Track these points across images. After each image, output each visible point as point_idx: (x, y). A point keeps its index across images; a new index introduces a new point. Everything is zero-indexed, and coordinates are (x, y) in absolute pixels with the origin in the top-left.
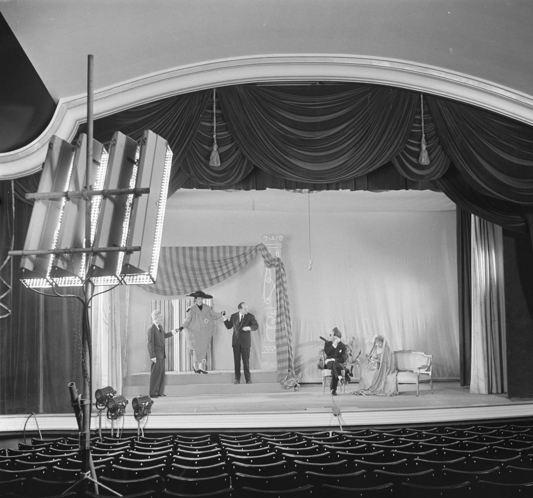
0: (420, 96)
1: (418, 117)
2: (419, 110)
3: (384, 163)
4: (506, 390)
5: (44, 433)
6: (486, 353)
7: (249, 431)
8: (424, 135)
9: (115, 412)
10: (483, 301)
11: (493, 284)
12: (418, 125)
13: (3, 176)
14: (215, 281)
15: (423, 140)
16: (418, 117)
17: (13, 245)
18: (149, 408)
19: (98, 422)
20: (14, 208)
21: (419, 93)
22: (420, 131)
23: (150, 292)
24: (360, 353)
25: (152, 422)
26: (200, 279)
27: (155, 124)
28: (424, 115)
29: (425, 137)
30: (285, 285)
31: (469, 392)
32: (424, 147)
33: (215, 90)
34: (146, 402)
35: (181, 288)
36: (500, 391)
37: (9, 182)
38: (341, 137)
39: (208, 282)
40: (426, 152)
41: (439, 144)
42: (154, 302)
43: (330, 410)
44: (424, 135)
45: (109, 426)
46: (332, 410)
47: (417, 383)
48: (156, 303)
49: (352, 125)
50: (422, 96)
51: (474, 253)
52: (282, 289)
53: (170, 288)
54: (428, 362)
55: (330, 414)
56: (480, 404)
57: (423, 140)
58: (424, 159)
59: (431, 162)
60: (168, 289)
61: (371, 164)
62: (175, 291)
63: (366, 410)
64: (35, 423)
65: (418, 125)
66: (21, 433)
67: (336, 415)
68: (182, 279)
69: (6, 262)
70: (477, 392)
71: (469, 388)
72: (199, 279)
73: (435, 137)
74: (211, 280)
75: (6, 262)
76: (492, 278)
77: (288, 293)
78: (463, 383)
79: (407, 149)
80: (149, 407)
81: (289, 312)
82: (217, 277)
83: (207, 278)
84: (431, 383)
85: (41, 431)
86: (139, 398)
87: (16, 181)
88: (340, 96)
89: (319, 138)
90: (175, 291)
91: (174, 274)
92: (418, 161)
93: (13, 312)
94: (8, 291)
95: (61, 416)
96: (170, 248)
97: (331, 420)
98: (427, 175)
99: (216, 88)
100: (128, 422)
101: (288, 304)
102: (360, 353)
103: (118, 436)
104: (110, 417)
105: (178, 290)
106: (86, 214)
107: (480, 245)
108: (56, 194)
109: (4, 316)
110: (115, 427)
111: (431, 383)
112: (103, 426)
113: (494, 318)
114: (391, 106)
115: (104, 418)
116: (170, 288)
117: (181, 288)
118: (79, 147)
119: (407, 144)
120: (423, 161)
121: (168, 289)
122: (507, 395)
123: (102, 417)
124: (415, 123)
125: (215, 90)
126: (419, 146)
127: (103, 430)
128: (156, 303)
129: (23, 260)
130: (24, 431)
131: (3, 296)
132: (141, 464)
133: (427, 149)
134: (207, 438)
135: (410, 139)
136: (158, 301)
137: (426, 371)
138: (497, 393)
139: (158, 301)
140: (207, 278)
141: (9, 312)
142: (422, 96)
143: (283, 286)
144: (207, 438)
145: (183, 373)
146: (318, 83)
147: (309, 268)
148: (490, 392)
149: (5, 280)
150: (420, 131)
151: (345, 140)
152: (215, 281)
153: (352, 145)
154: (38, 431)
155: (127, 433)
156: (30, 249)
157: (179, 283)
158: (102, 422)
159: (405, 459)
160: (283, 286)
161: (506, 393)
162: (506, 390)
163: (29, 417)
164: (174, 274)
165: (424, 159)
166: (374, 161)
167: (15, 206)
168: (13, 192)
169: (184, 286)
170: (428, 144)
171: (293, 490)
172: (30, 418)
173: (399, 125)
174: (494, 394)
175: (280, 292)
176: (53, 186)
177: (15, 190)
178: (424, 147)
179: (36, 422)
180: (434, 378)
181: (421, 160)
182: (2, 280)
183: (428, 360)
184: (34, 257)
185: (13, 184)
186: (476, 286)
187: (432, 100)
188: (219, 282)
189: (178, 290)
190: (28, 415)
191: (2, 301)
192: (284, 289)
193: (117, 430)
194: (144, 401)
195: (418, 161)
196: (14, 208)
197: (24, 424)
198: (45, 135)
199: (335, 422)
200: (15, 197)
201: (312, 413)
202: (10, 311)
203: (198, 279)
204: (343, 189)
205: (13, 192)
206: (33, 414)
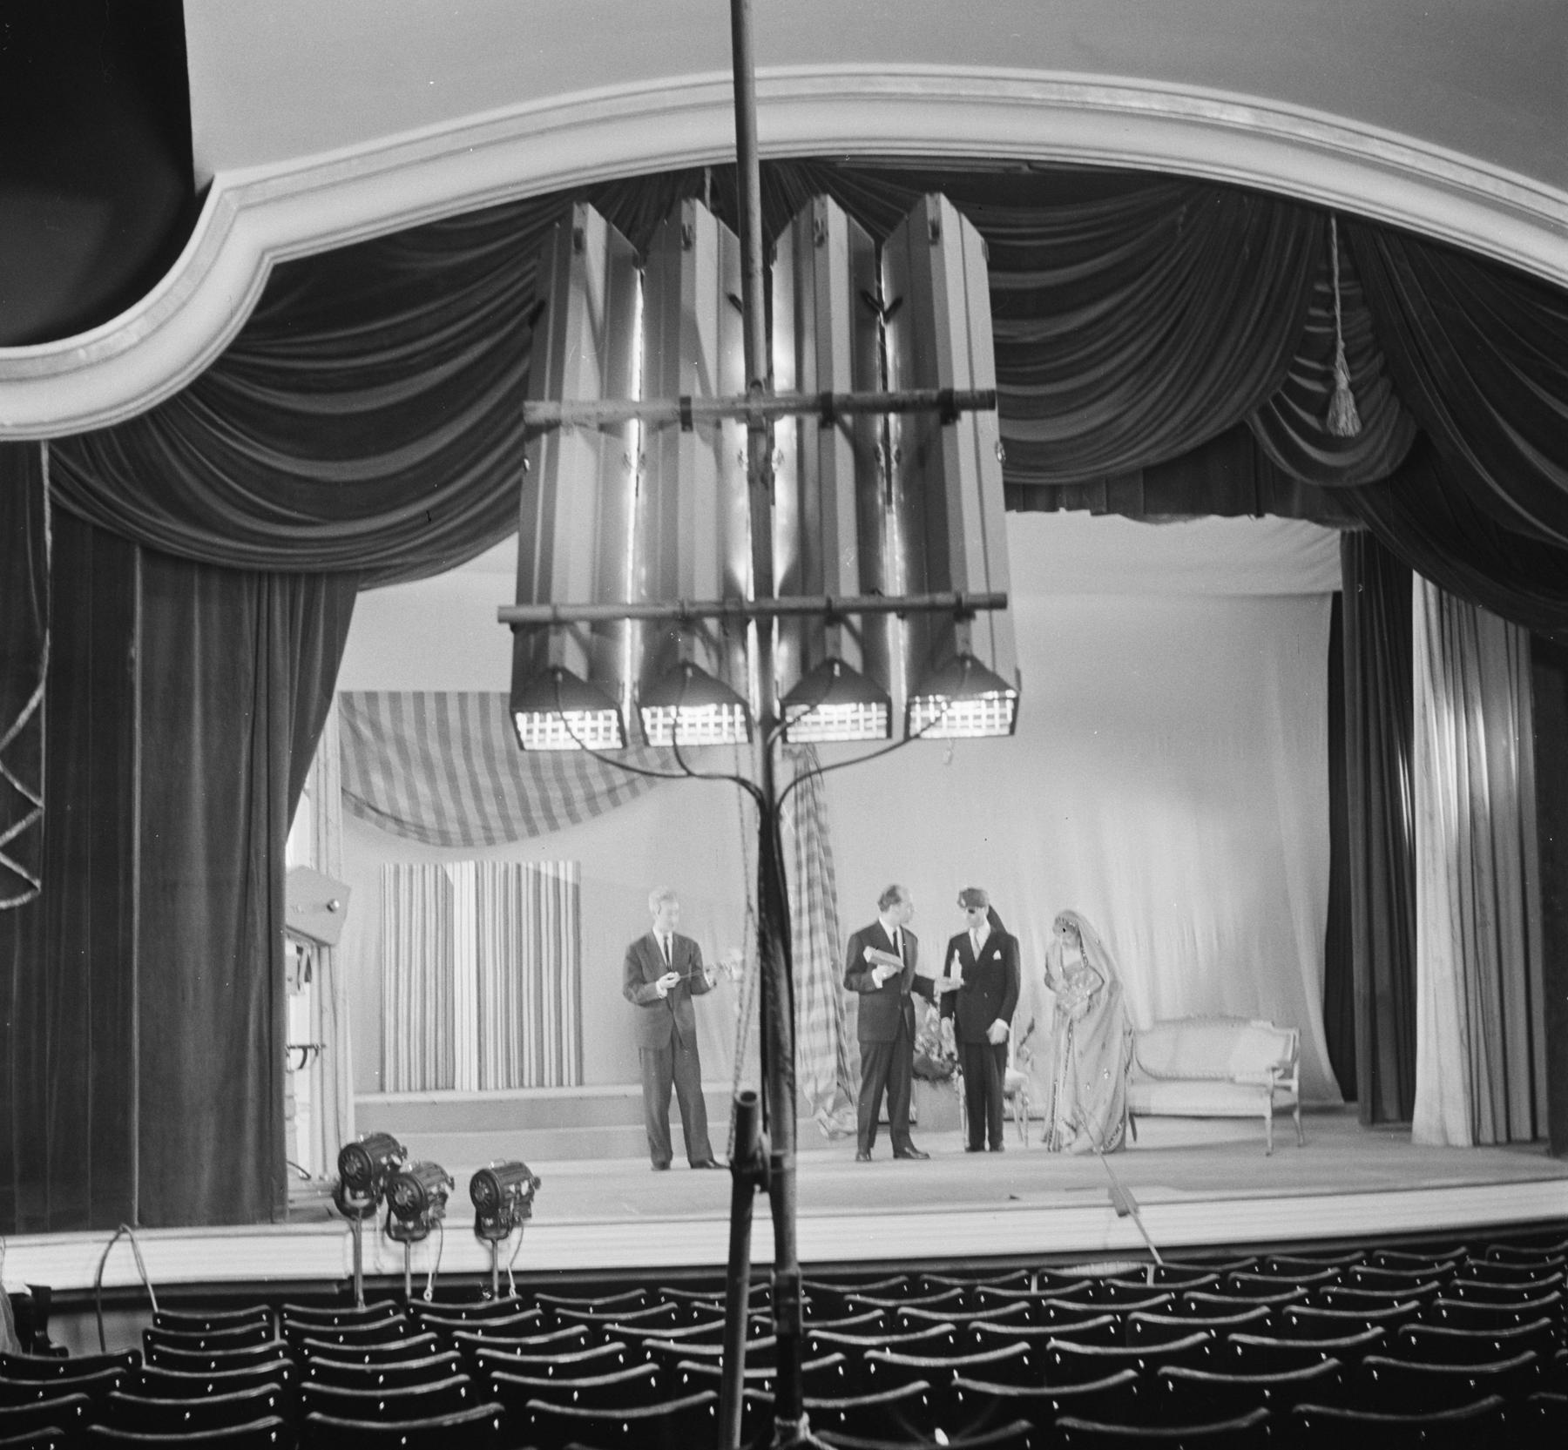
0: (1328, 222)
1: (1321, 287)
2: (1323, 267)
3: (1227, 426)
4: (1543, 1130)
5: (164, 1293)
6: (1463, 1023)
7: (896, 1269)
8: (1341, 344)
9: (414, 1218)
10: (1454, 867)
11: (1479, 813)
12: (1320, 313)
13: (16, 426)
14: (603, 802)
15: (1340, 358)
16: (1321, 287)
17: (46, 662)
18: (528, 1204)
19: (350, 1251)
20: (48, 536)
21: (1323, 212)
22: (1327, 330)
23: (400, 834)
24: (1031, 1029)
25: (538, 1247)
26: (559, 794)
27: (517, 275)
28: (1340, 281)
29: (1345, 351)
30: (822, 817)
31: (1408, 1141)
32: (1343, 380)
33: (708, 174)
34: (518, 1184)
35: (496, 824)
36: (1502, 1138)
37: (33, 447)
38: (1097, 340)
39: (580, 806)
40: (1351, 395)
41: (1384, 371)
42: (390, 868)
43: (1102, 1196)
44: (1341, 344)
45: (390, 1266)
46: (1111, 1196)
47: (1268, 1114)
48: (397, 873)
49: (1133, 303)
50: (1334, 223)
51: (1425, 717)
52: (814, 827)
53: (463, 822)
54: (1285, 1051)
55: (1103, 1210)
56: (1440, 1180)
57: (1340, 358)
58: (1346, 419)
59: (1364, 424)
60: (453, 828)
61: (1188, 427)
62: (477, 833)
63: (1212, 1195)
64: (133, 1261)
65: (1320, 313)
66: (134, 1294)
67: (1122, 1214)
68: (499, 793)
69: (24, 717)
70: (1436, 1140)
71: (1410, 1130)
72: (555, 794)
73: (1370, 352)
74: (591, 798)
75: (24, 717)
76: (1477, 793)
77: (832, 841)
78: (1369, 1116)
79: (1291, 387)
80: (525, 1202)
81: (834, 900)
82: (611, 791)
83: (578, 793)
84: (1296, 1115)
85: (156, 1287)
86: (496, 1170)
87: (56, 443)
88: (1094, 210)
89: (1031, 339)
90: (477, 833)
91: (473, 776)
92: (1323, 424)
93: (43, 886)
94: (32, 817)
95: (223, 1236)
96: (462, 696)
97: (1108, 1230)
98: (1352, 467)
99: (714, 168)
100: (453, 1248)
101: (831, 875)
102: (1031, 1029)
103: (428, 1295)
104: (418, 1234)
105: (487, 828)
106: (751, 481)
107: (1442, 694)
108: (608, 409)
109: (17, 902)
110: (503, 1263)
111: (1296, 1115)
112: (368, 1267)
113: (1484, 915)
114: (1247, 250)
115: (371, 1232)
116: (463, 822)
117: (496, 824)
118: (689, 244)
119: (1293, 371)
120: (1342, 424)
121: (453, 828)
122: (1548, 1146)
123: (364, 1235)
124: (1314, 305)
125: (708, 174)
126: (1328, 378)
127: (367, 1278)
128: (397, 873)
129: (553, 640)
130: (98, 1288)
131: (11, 834)
132: (210, 1388)
133: (1351, 385)
134: (256, 1317)
135: (1299, 355)
136: (404, 868)
137: (1282, 1077)
138: (1496, 1144)
139: (404, 868)
140: (578, 793)
141: (32, 887)
142: (1334, 223)
143: (817, 820)
144: (256, 1317)
145: (484, 1096)
146: (1026, 168)
147: (946, 759)
148: (1477, 1142)
149: (21, 780)
150: (1327, 330)
151: (1111, 349)
152: (603, 802)
153: (1131, 366)
154: (144, 1287)
155: (459, 1290)
156: (570, 601)
157: (491, 808)
158: (364, 1250)
159: (1531, 1354)
160: (817, 820)
161: (1544, 1141)
162: (1543, 1130)
163: (111, 1243)
164: (473, 776)
165: (1346, 419)
166: (1199, 418)
167: (52, 529)
168: (46, 482)
169: (505, 818)
170: (1352, 372)
171: (138, 1436)
172: (116, 1245)
173: (1134, 331)
174: (1488, 1145)
175: (809, 837)
176: (602, 381)
177: (51, 478)
178: (1343, 380)
179: (137, 1256)
180: (1305, 1102)
181: (1336, 421)
182: (10, 778)
183: (1287, 1044)
184: (584, 628)
185: (45, 456)
186: (1431, 818)
187: (1369, 238)
188: (616, 803)
189: (487, 828)
190: (110, 1235)
191: (8, 849)
192: (821, 829)
193: (424, 1276)
194: (515, 1178)
195: (1323, 424)
196: (48, 536)
197: (97, 1263)
198: (165, 295)
199: (1124, 1234)
200: (53, 505)
201: (1049, 1208)
202: (37, 883)
203: (551, 794)
204: (1069, 508)
205: (46, 482)
206: (125, 1231)
